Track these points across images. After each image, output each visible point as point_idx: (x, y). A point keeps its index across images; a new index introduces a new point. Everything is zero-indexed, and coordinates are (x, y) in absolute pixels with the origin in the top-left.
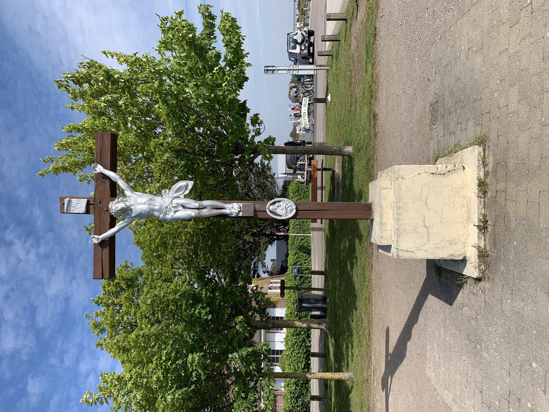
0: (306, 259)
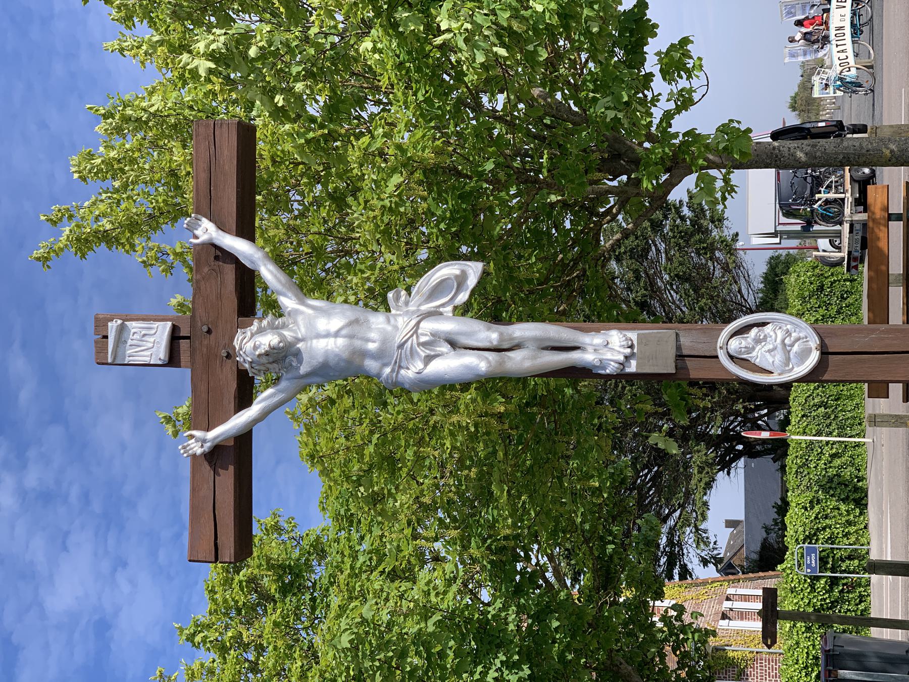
0: (849, 523)
